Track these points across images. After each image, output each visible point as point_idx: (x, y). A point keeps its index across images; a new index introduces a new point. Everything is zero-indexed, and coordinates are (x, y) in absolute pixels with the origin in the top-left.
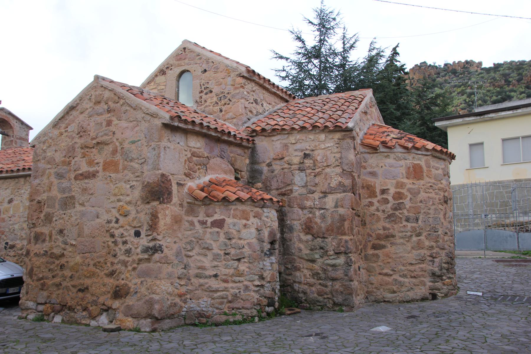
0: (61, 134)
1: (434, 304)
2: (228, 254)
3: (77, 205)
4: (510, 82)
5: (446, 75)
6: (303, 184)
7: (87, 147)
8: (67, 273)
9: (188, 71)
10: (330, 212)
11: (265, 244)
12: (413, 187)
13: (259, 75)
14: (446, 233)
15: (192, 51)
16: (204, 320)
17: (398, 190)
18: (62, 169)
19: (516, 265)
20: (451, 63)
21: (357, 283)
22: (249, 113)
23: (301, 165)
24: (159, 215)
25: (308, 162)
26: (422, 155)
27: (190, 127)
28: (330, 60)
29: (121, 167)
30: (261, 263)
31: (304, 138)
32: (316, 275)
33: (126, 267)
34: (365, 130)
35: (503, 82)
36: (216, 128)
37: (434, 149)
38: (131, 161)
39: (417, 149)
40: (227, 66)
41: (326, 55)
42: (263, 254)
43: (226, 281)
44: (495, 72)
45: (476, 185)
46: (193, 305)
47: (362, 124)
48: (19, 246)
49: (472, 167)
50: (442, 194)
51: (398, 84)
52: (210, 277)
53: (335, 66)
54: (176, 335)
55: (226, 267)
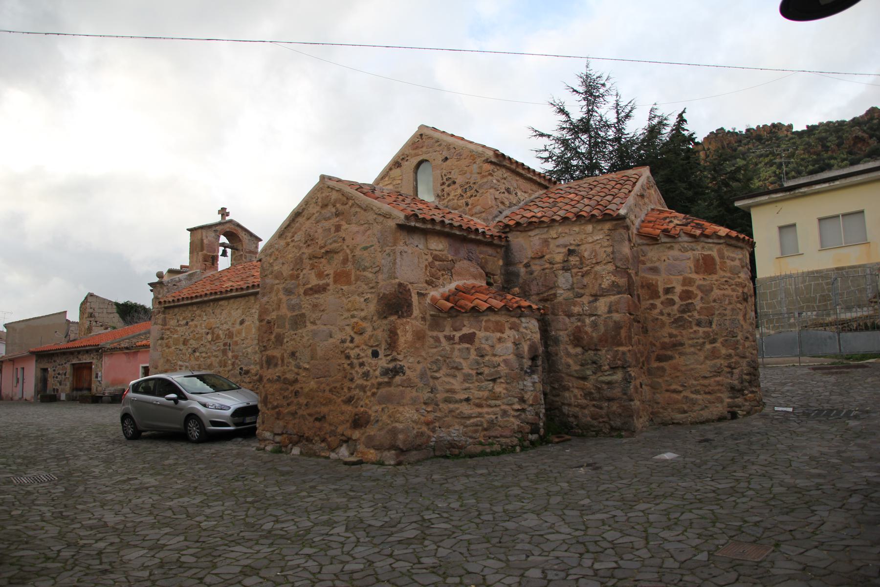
0: (288, 244)
1: (734, 424)
2: (481, 374)
3: (308, 324)
4: (828, 147)
5: (749, 142)
6: (569, 287)
7: (316, 257)
8: (303, 400)
9: (427, 161)
10: (602, 318)
11: (525, 360)
12: (705, 283)
13: (510, 159)
14: (747, 338)
15: (430, 138)
16: (456, 451)
17: (686, 288)
18: (291, 284)
19: (836, 373)
20: (755, 128)
21: (638, 403)
22: (500, 205)
23: (566, 264)
24: (399, 332)
25: (574, 260)
26: (713, 243)
27: (429, 226)
28: (602, 134)
29: (353, 278)
30: (521, 382)
31: (567, 231)
32: (588, 395)
33: (365, 392)
34: (643, 217)
35: (820, 148)
36: (461, 226)
37: (728, 236)
38: (364, 270)
39: (707, 236)
40: (472, 151)
41: (597, 128)
42: (523, 373)
43: (479, 406)
44: (809, 136)
45: (790, 276)
46: (442, 434)
47: (638, 209)
48: (253, 372)
49: (783, 255)
50: (740, 290)
51: (688, 158)
52: (461, 401)
53: (609, 140)
54: (423, 469)
55: (480, 389)
